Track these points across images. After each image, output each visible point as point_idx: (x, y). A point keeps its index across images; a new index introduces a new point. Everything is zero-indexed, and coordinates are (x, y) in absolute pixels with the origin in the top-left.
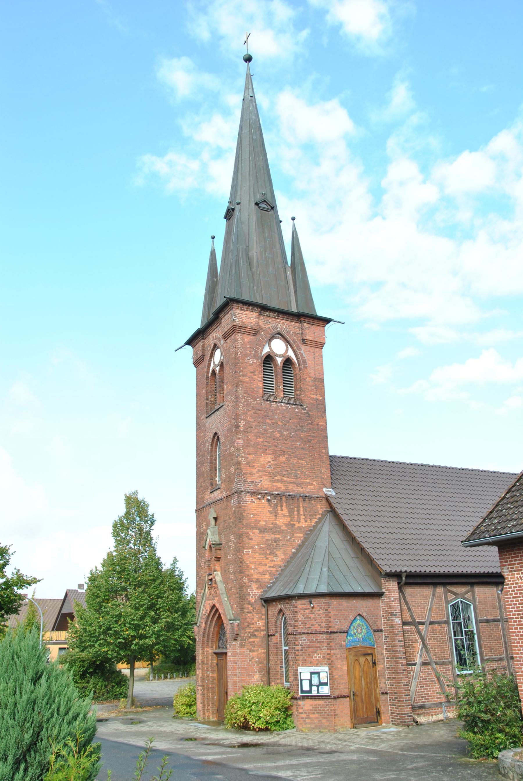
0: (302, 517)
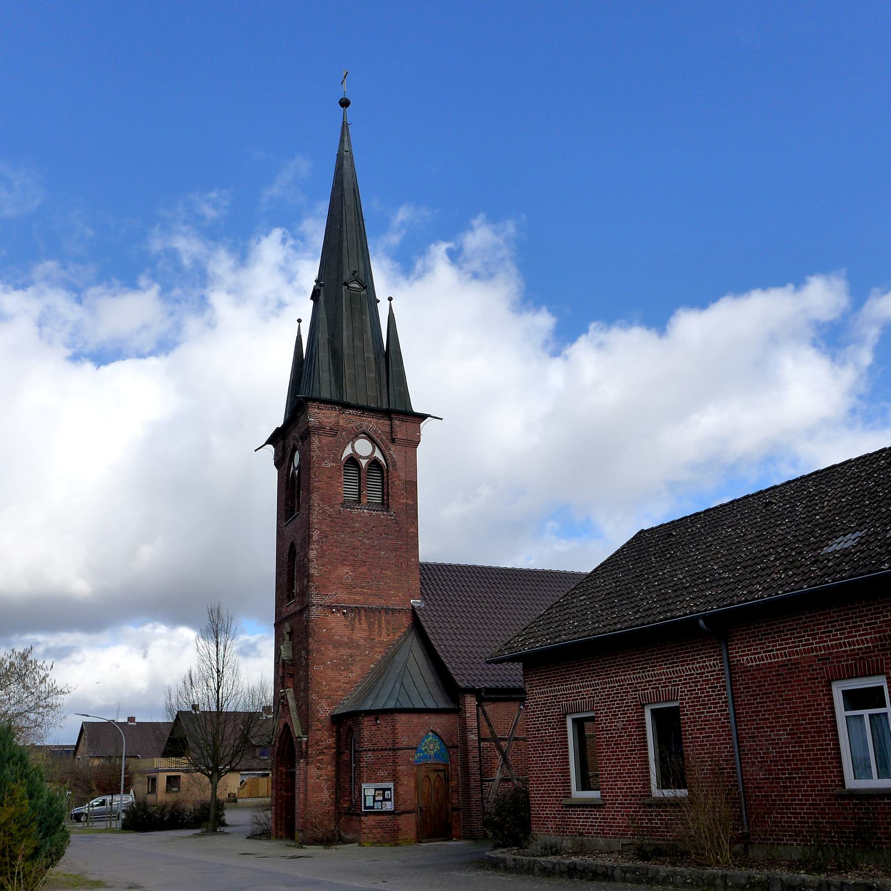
0: (384, 631)
